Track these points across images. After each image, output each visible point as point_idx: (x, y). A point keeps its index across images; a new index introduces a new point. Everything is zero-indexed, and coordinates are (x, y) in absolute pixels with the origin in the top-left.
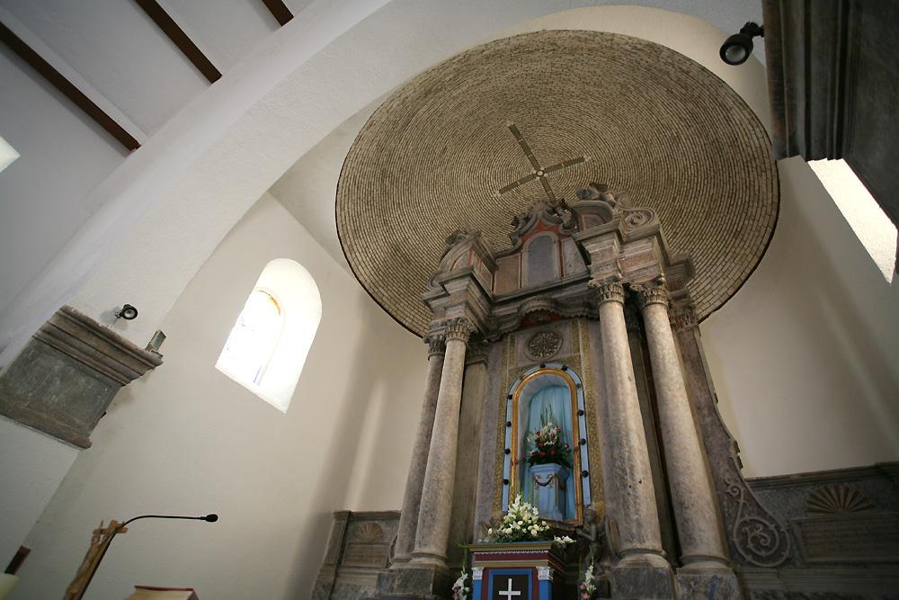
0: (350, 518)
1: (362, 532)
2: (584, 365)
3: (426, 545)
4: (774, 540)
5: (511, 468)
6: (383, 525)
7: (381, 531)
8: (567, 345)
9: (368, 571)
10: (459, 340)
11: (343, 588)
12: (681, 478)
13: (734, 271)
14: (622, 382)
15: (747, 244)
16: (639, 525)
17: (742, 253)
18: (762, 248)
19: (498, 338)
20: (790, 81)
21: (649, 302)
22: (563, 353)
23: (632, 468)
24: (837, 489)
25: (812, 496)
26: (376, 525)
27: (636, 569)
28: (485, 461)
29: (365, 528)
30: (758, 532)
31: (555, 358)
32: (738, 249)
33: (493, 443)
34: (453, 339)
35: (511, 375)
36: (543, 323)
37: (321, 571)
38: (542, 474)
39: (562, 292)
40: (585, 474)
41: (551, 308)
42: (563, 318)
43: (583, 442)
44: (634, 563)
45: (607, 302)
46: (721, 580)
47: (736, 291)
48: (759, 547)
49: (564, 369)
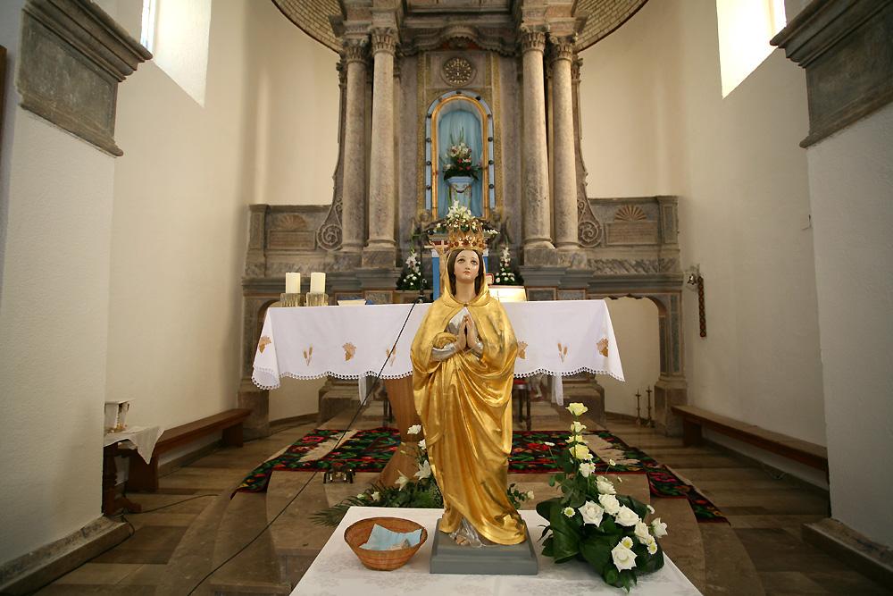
0: (268, 210)
1: (282, 221)
2: (494, 98)
3: (383, 234)
4: (595, 233)
5: (432, 177)
6: (304, 217)
7: (304, 222)
8: (480, 76)
9: (298, 253)
10: (389, 53)
11: (275, 266)
12: (564, 197)
13: (596, 27)
14: (539, 124)
15: (616, 7)
16: (542, 225)
17: (608, 13)
18: (627, 15)
19: (412, 53)
20: (819, 15)
21: (561, 57)
22: (477, 83)
23: (541, 188)
24: (632, 208)
25: (620, 211)
26: (297, 216)
27: (539, 250)
28: (405, 169)
29: (286, 219)
30: (588, 229)
31: (469, 86)
32: (608, 9)
33: (412, 155)
34: (384, 52)
35: (428, 95)
36: (460, 48)
37: (248, 254)
38: (458, 184)
39: (477, 18)
40: (491, 187)
41: (474, 37)
42: (481, 49)
43: (490, 163)
44: (538, 246)
45: (534, 50)
46: (579, 255)
47: (590, 45)
48: (587, 237)
49: (478, 99)
